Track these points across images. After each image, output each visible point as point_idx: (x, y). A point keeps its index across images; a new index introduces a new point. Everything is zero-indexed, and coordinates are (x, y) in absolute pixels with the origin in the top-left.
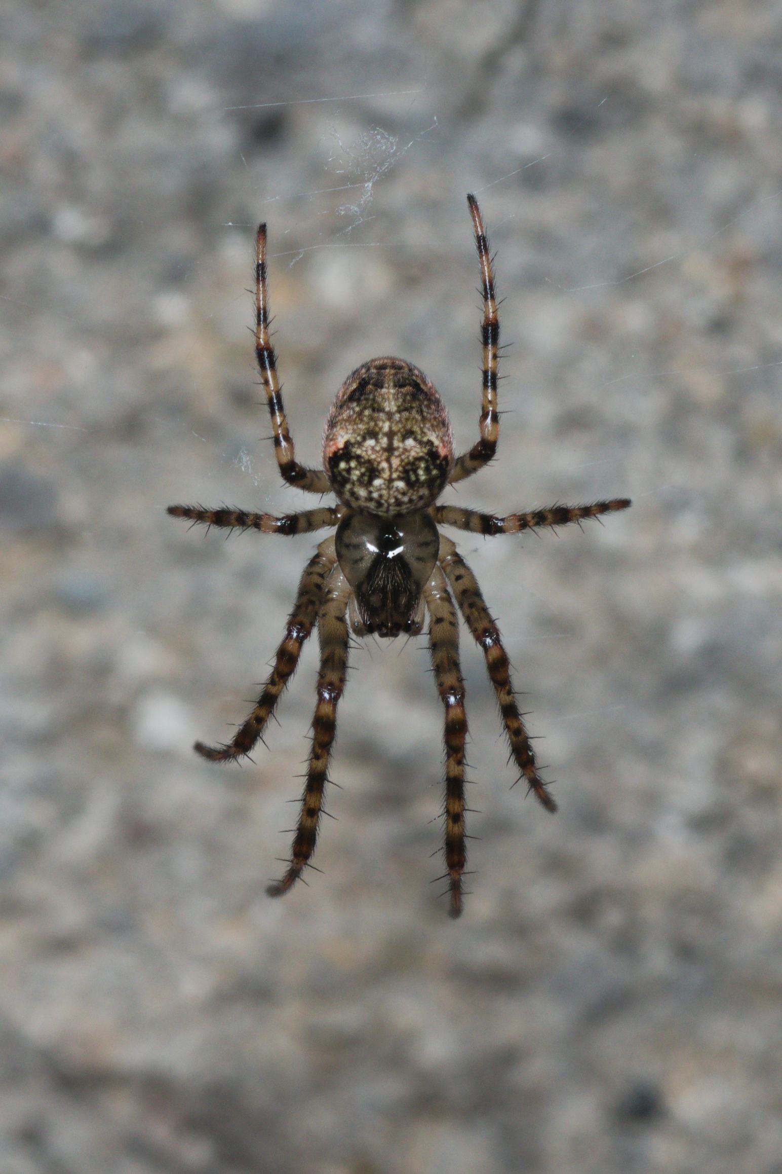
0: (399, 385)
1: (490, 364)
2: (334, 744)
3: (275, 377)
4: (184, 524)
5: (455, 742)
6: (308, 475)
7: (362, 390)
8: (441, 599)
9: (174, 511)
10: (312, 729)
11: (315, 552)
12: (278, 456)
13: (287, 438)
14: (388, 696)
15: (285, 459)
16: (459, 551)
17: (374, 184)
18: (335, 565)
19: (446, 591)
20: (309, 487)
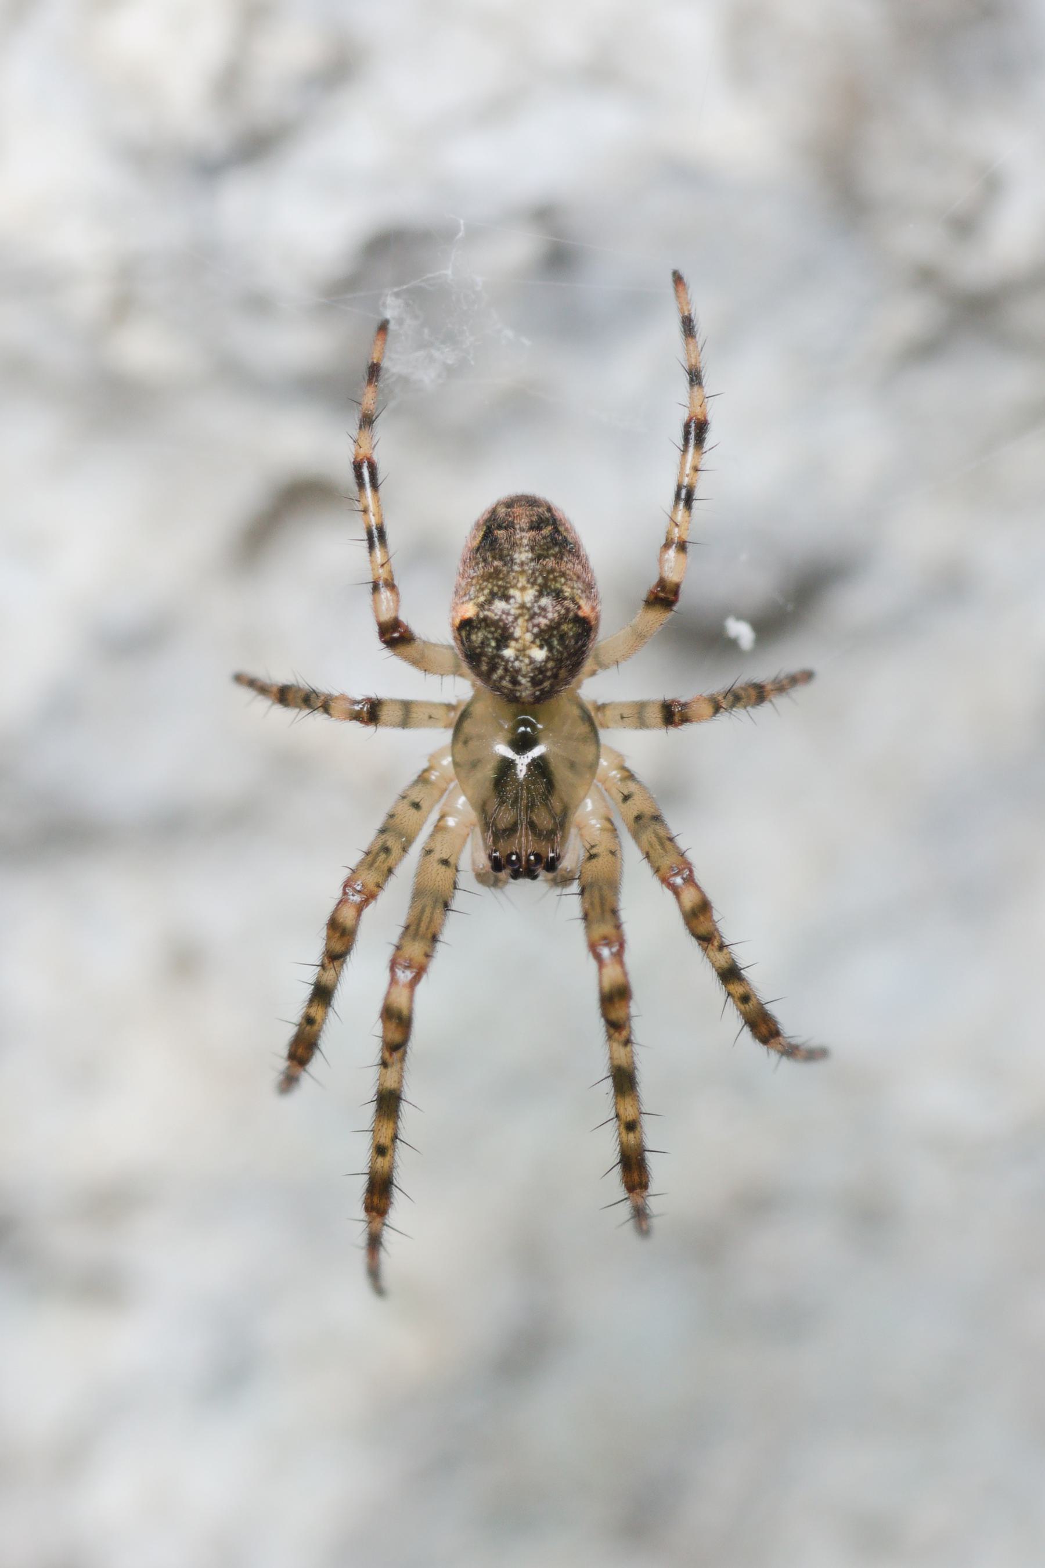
0: (536, 526)
1: (685, 308)
2: (410, 1044)
3: (377, 501)
4: (247, 694)
5: (702, 929)
6: (418, 642)
7: (493, 536)
8: (602, 829)
9: (240, 679)
10: (380, 1020)
11: (425, 765)
12: (376, 610)
13: (391, 586)
14: (511, 947)
15: (386, 616)
16: (627, 764)
17: (538, 722)
18: (452, 785)
19: (609, 820)
20: (421, 663)
